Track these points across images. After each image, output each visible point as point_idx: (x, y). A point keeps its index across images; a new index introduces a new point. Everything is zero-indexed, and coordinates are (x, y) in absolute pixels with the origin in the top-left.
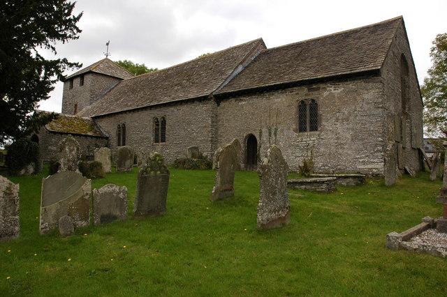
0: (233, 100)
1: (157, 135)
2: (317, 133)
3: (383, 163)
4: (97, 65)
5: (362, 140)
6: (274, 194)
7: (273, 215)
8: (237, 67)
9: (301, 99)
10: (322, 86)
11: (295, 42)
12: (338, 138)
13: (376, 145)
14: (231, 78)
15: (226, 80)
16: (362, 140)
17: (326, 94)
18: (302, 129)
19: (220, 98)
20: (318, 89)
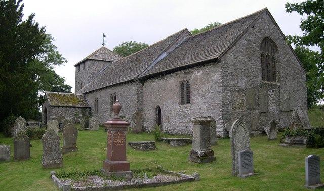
0: (149, 81)
1: (182, 98)
2: (190, 105)
3: (222, 128)
4: (91, 56)
5: (212, 110)
6: (51, 151)
7: (51, 162)
8: (162, 53)
9: (181, 80)
10: (191, 70)
11: (233, 20)
12: (200, 109)
13: (219, 114)
14: (155, 63)
15: (150, 66)
16: (212, 110)
17: (193, 76)
18: (182, 103)
19: (143, 80)
20: (189, 73)
